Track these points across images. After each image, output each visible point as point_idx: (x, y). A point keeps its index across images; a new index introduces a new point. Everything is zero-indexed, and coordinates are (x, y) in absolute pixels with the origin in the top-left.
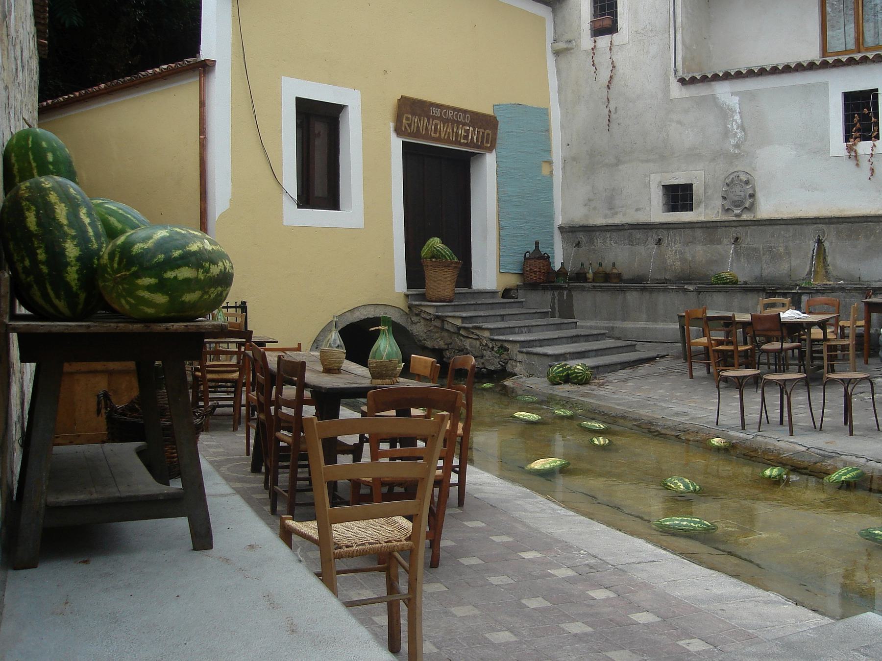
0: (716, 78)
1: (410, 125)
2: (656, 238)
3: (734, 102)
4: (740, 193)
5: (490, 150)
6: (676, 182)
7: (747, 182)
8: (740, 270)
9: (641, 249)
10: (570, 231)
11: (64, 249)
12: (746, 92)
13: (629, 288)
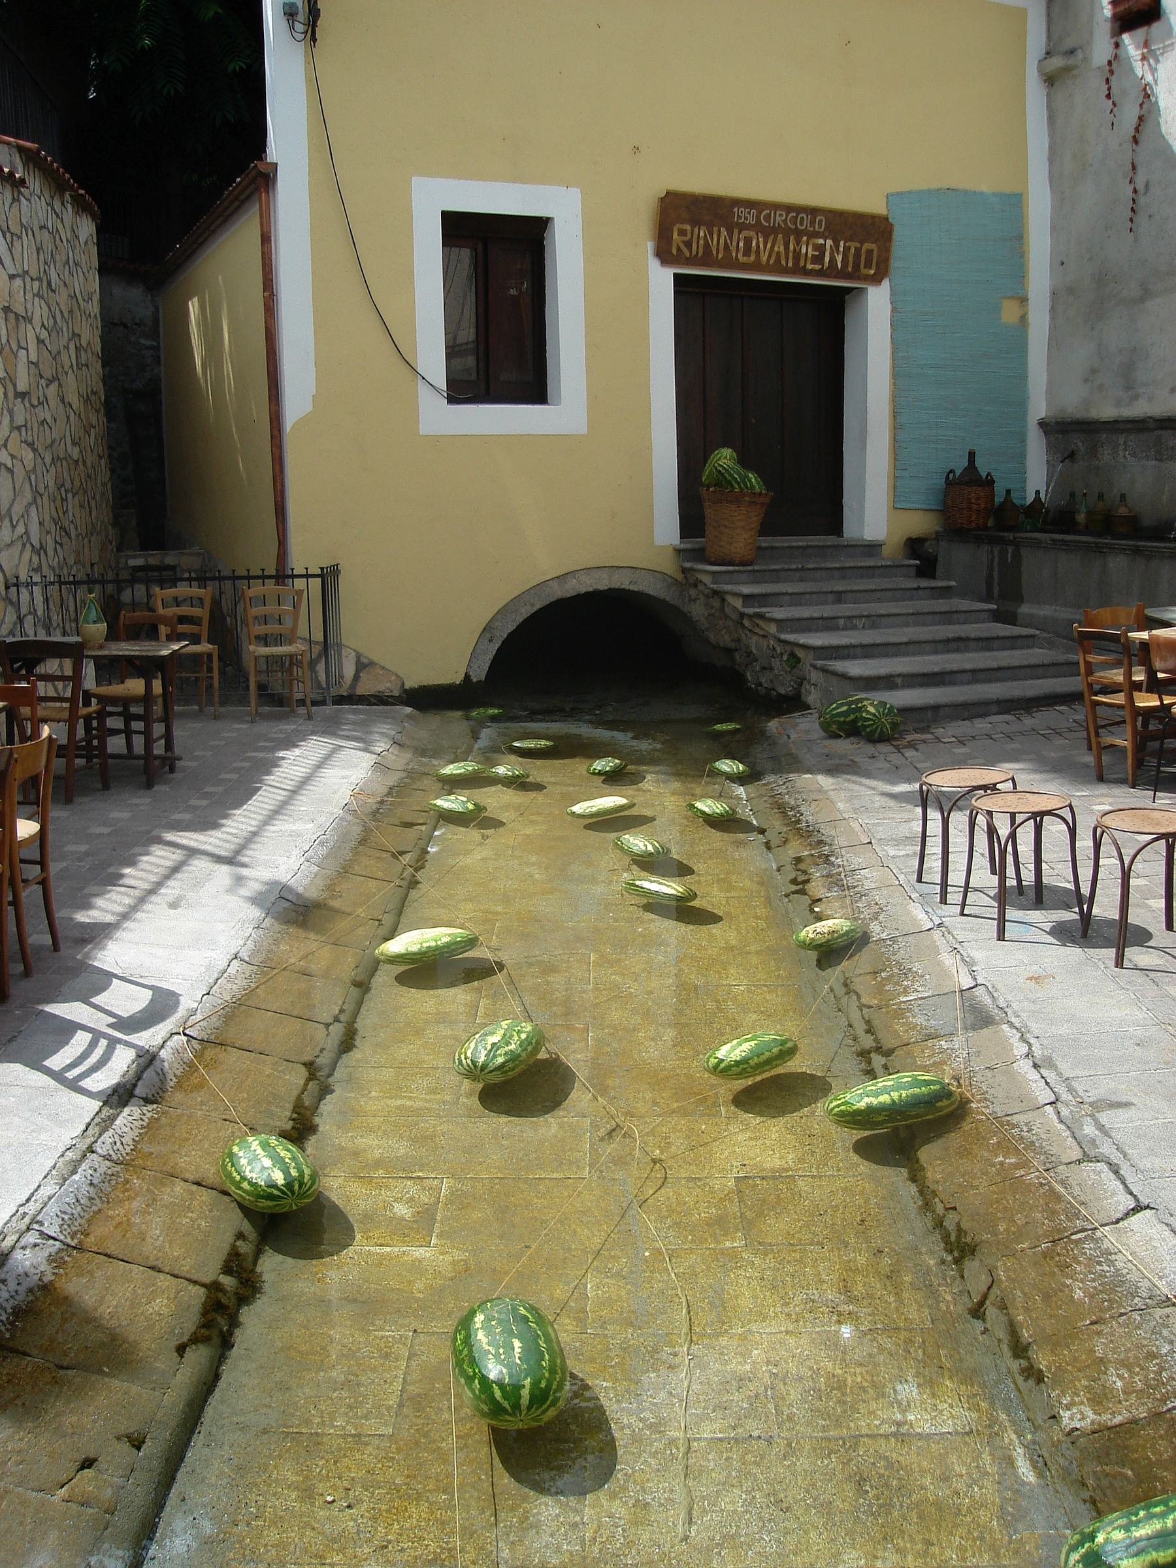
1: (689, 245)
5: (877, 280)
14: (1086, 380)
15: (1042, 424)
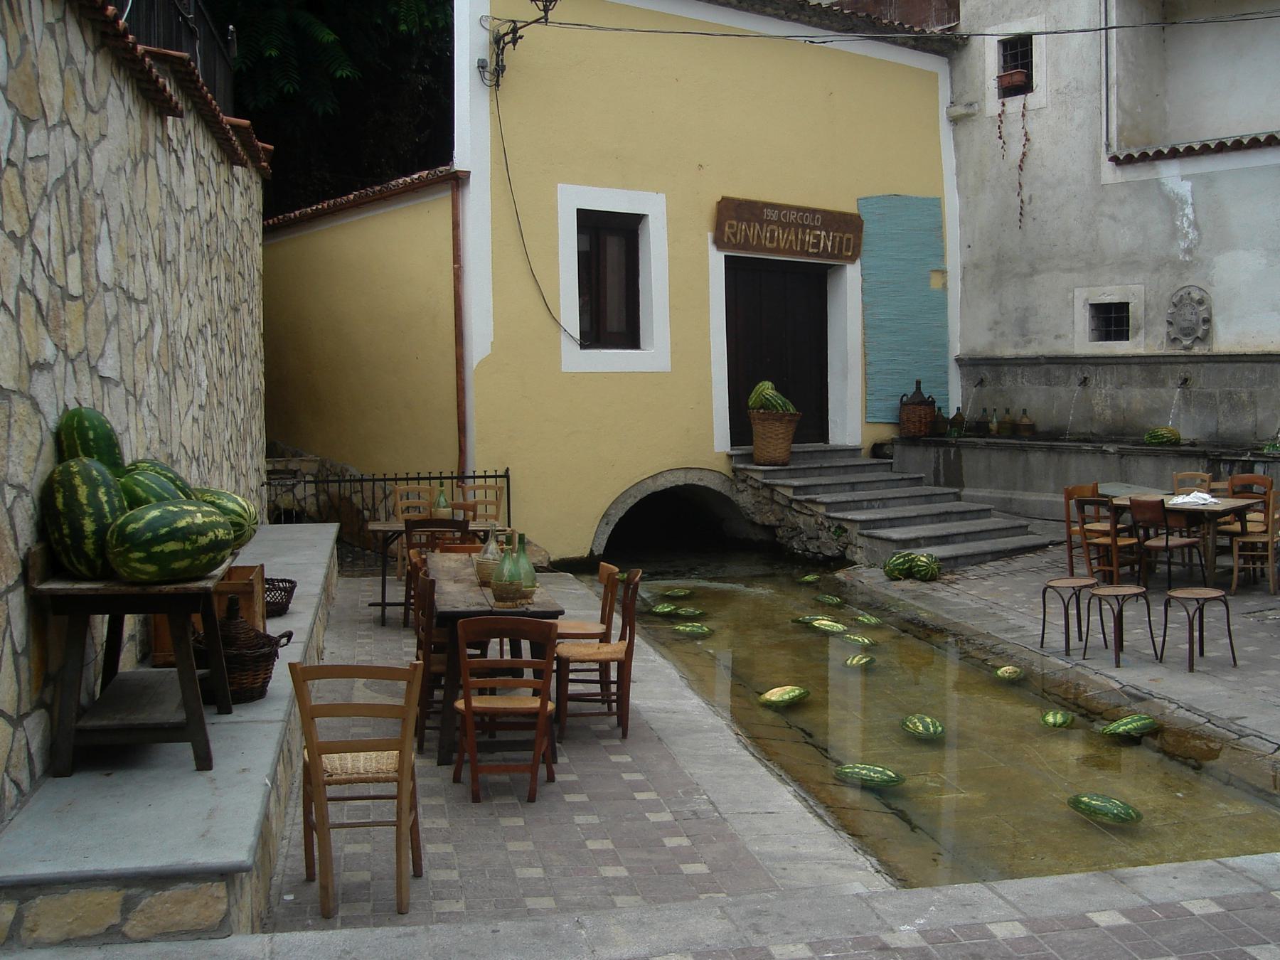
0: (1159, 156)
1: (735, 235)
2: (1081, 376)
3: (1185, 188)
4: (1191, 315)
5: (852, 259)
6: (1107, 300)
7: (1200, 302)
8: (1184, 424)
9: (1061, 390)
10: (972, 365)
11: (82, 525)
12: (1201, 175)
13: (1032, 447)
14: (990, 329)
15: (958, 360)
